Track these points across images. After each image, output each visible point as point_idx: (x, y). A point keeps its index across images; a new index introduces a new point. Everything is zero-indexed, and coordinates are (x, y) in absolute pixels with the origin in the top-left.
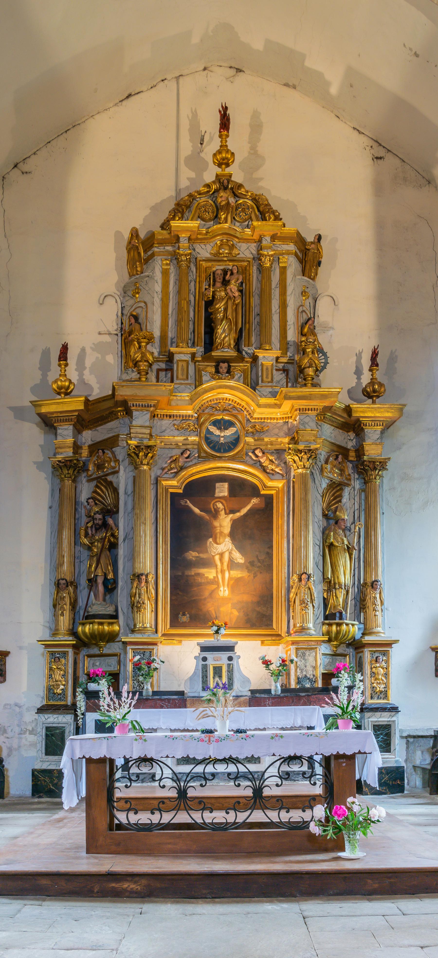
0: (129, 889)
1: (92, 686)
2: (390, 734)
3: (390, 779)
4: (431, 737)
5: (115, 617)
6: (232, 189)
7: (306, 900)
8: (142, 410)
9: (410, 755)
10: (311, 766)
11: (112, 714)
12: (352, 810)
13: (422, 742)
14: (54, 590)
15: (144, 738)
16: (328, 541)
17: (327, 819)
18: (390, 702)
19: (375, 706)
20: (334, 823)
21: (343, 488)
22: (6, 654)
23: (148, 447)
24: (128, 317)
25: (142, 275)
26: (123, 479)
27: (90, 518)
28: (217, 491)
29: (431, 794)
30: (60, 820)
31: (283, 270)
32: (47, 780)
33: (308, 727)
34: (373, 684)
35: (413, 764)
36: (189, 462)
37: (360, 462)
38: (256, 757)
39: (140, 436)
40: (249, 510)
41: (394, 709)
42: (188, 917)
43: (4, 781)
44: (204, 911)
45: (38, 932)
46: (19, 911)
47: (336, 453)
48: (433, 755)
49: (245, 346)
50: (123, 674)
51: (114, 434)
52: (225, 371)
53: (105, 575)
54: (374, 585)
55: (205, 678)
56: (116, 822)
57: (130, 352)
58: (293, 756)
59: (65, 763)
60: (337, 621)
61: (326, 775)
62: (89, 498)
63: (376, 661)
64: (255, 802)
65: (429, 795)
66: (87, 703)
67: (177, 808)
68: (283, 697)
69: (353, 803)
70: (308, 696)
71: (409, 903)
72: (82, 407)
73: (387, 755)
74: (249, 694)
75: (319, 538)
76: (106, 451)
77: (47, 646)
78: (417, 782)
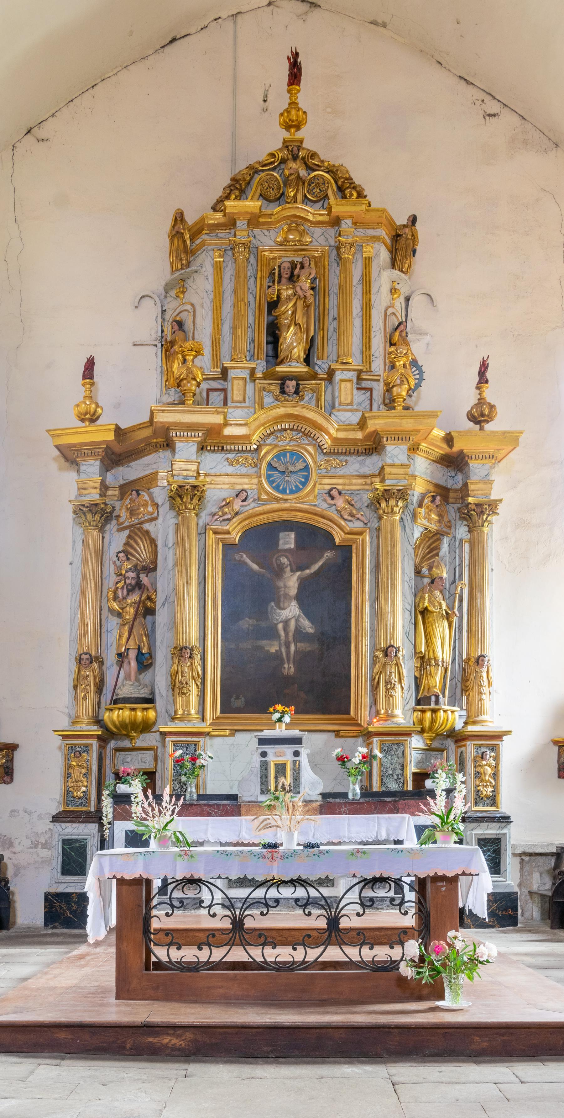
0: (170, 1045)
1: (122, 788)
2: (500, 851)
3: (498, 908)
4: (552, 854)
5: (150, 701)
6: (303, 158)
7: (395, 1062)
8: (187, 441)
9: (524, 877)
10: (399, 889)
11: (149, 823)
12: (453, 947)
13: (541, 861)
14: (74, 667)
15: (190, 854)
16: (421, 605)
17: (422, 959)
18: (500, 810)
19: (480, 815)
20: (431, 963)
21: (442, 537)
22: (11, 748)
23: (194, 487)
24: (170, 323)
25: (188, 270)
26: (163, 528)
27: (120, 577)
28: (281, 542)
29: (552, 928)
30: (81, 957)
31: (368, 262)
32: (64, 905)
33: (394, 840)
34: (478, 786)
35: (528, 890)
36: (246, 506)
37: (464, 504)
38: (331, 878)
39: (185, 473)
40: (322, 567)
41: (505, 820)
42: (245, 1082)
43: (9, 908)
44: (265, 1075)
45: (56, 1099)
46: (32, 1072)
47: (432, 494)
48: (554, 878)
49: (318, 359)
50: (160, 772)
51: (151, 471)
52: (293, 390)
53: (139, 649)
54: (479, 660)
55: (264, 778)
56: (153, 959)
57: (172, 367)
58: (379, 878)
59: (90, 885)
60: (433, 706)
61: (420, 902)
62: (120, 552)
63: (482, 758)
64: (330, 935)
65: (549, 929)
66: (115, 810)
67: (231, 942)
68: (363, 803)
69: (455, 938)
70: (395, 801)
71: (528, 1067)
72: (111, 436)
73: (496, 877)
74: (320, 798)
75: (410, 602)
76: (142, 493)
77: (65, 737)
78: (534, 913)
